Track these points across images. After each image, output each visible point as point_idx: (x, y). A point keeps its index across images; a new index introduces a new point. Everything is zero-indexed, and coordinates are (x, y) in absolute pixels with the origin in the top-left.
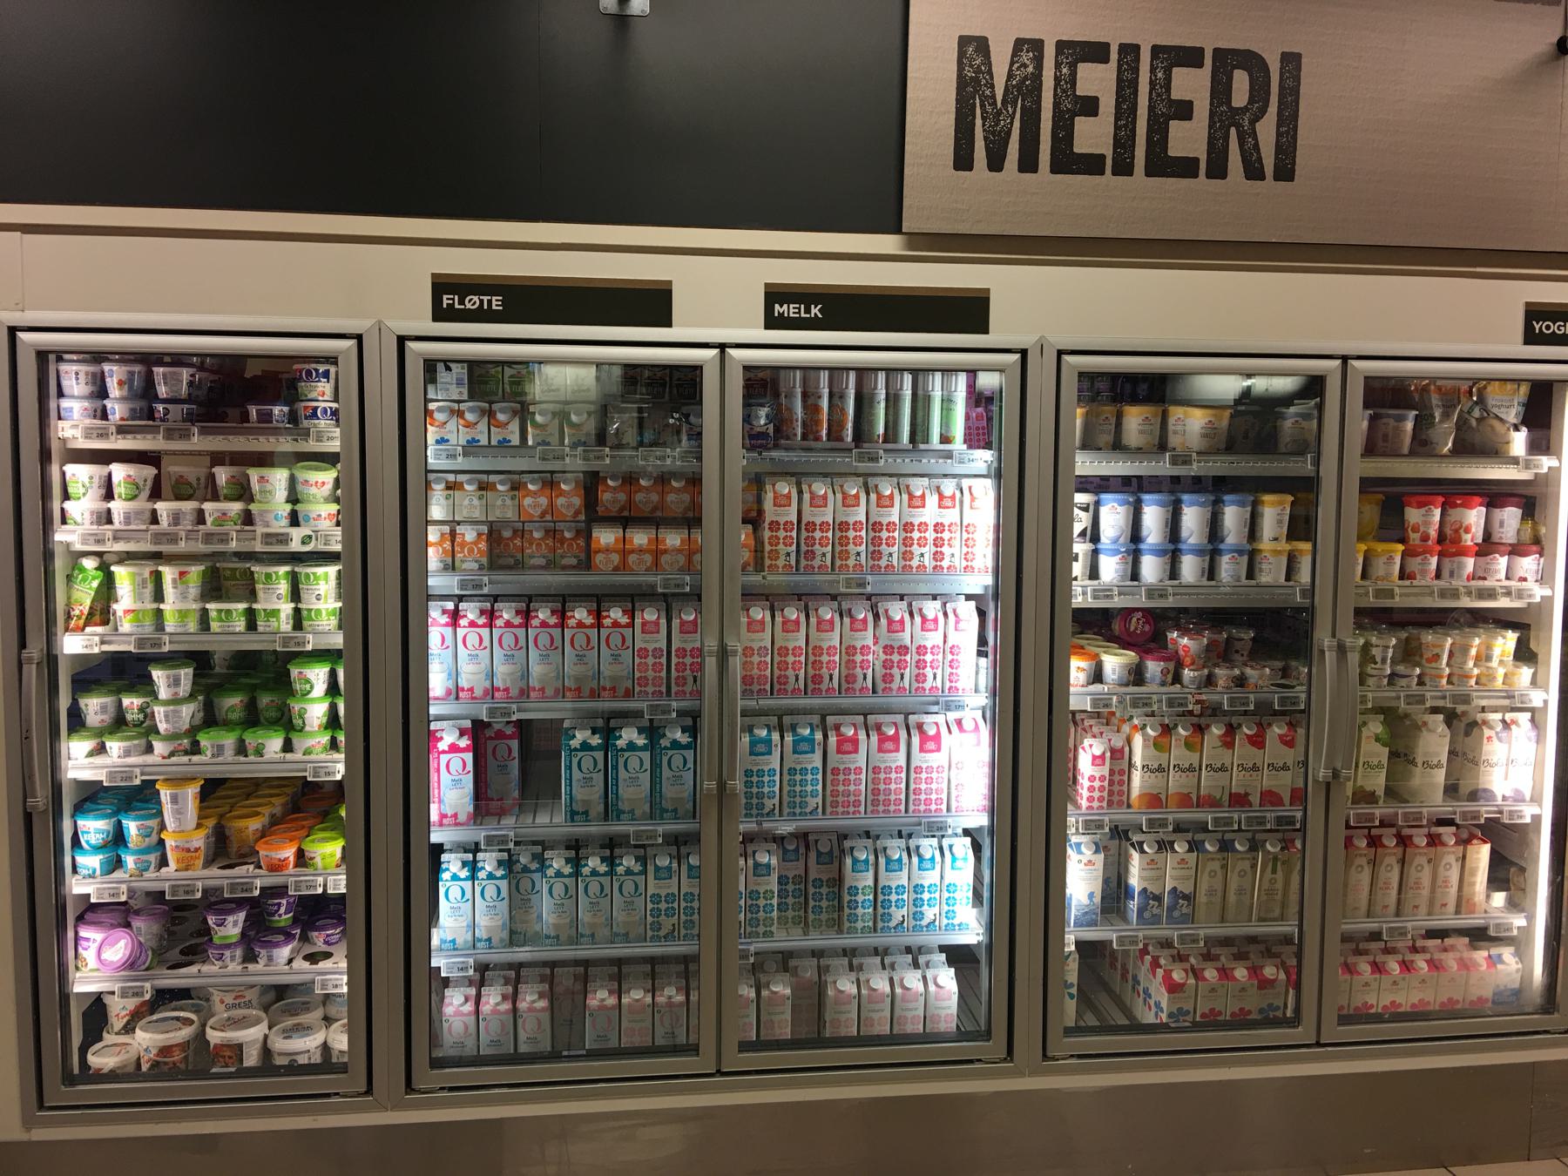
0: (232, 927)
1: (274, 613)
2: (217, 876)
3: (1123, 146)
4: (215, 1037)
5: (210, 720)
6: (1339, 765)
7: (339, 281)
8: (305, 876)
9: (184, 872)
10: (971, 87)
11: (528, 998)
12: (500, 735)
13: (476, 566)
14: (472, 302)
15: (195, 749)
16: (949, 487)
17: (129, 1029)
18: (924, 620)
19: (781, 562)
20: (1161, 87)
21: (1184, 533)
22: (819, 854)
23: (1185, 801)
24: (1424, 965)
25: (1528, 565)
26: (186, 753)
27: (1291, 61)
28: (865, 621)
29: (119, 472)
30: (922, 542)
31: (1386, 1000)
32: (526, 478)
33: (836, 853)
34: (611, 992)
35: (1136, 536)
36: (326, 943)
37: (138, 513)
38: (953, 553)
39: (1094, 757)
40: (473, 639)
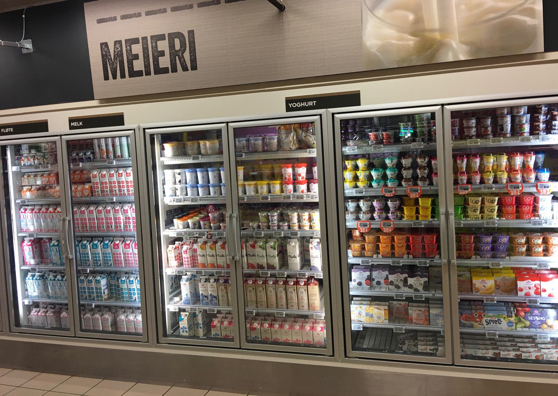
3: (193, 61)
10: (105, 57)
20: (155, 48)
23: (213, 266)
30: (123, 187)
31: (294, 339)
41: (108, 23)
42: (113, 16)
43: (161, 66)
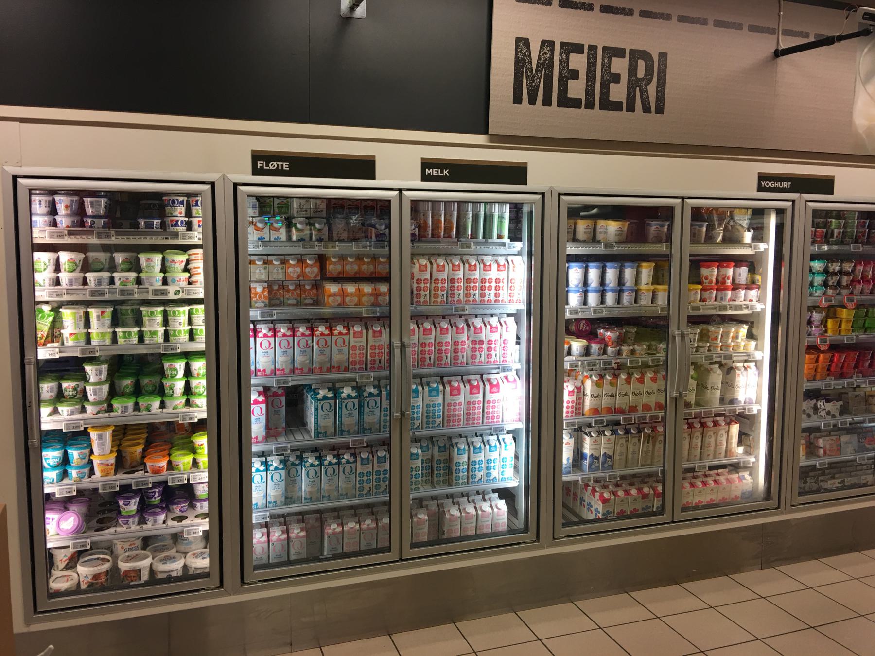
0: (133, 506)
1: (155, 333)
2: (123, 478)
4: (124, 566)
5: (113, 393)
6: (681, 390)
7: (198, 153)
8: (175, 474)
9: (102, 478)
10: (521, 63)
11: (296, 531)
12: (275, 394)
13: (263, 305)
14: (273, 165)
15: (110, 409)
16: (502, 260)
17: (71, 565)
18: (491, 327)
19: (439, 300)
20: (607, 67)
21: (607, 281)
22: (440, 447)
23: (610, 411)
24: (712, 482)
25: (753, 294)
26: (106, 411)
27: (663, 56)
28: (463, 328)
29: (65, 257)
30: (475, 288)
31: (696, 501)
32: (287, 258)
33: (447, 446)
34: (338, 525)
35: (585, 282)
36: (181, 511)
37: (76, 279)
38: (504, 294)
39: (570, 392)
40: (265, 344)
41: (619, 16)
42: (804, 30)
43: (571, 94)
